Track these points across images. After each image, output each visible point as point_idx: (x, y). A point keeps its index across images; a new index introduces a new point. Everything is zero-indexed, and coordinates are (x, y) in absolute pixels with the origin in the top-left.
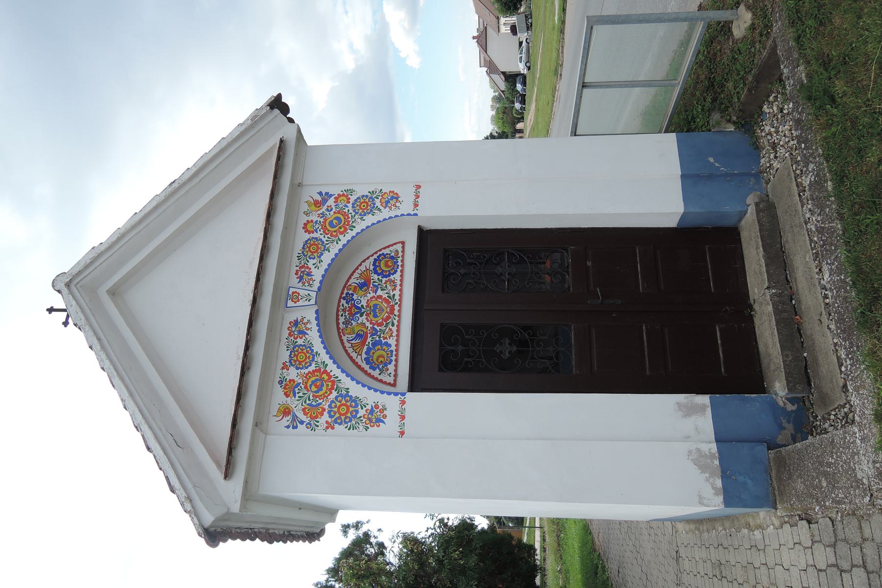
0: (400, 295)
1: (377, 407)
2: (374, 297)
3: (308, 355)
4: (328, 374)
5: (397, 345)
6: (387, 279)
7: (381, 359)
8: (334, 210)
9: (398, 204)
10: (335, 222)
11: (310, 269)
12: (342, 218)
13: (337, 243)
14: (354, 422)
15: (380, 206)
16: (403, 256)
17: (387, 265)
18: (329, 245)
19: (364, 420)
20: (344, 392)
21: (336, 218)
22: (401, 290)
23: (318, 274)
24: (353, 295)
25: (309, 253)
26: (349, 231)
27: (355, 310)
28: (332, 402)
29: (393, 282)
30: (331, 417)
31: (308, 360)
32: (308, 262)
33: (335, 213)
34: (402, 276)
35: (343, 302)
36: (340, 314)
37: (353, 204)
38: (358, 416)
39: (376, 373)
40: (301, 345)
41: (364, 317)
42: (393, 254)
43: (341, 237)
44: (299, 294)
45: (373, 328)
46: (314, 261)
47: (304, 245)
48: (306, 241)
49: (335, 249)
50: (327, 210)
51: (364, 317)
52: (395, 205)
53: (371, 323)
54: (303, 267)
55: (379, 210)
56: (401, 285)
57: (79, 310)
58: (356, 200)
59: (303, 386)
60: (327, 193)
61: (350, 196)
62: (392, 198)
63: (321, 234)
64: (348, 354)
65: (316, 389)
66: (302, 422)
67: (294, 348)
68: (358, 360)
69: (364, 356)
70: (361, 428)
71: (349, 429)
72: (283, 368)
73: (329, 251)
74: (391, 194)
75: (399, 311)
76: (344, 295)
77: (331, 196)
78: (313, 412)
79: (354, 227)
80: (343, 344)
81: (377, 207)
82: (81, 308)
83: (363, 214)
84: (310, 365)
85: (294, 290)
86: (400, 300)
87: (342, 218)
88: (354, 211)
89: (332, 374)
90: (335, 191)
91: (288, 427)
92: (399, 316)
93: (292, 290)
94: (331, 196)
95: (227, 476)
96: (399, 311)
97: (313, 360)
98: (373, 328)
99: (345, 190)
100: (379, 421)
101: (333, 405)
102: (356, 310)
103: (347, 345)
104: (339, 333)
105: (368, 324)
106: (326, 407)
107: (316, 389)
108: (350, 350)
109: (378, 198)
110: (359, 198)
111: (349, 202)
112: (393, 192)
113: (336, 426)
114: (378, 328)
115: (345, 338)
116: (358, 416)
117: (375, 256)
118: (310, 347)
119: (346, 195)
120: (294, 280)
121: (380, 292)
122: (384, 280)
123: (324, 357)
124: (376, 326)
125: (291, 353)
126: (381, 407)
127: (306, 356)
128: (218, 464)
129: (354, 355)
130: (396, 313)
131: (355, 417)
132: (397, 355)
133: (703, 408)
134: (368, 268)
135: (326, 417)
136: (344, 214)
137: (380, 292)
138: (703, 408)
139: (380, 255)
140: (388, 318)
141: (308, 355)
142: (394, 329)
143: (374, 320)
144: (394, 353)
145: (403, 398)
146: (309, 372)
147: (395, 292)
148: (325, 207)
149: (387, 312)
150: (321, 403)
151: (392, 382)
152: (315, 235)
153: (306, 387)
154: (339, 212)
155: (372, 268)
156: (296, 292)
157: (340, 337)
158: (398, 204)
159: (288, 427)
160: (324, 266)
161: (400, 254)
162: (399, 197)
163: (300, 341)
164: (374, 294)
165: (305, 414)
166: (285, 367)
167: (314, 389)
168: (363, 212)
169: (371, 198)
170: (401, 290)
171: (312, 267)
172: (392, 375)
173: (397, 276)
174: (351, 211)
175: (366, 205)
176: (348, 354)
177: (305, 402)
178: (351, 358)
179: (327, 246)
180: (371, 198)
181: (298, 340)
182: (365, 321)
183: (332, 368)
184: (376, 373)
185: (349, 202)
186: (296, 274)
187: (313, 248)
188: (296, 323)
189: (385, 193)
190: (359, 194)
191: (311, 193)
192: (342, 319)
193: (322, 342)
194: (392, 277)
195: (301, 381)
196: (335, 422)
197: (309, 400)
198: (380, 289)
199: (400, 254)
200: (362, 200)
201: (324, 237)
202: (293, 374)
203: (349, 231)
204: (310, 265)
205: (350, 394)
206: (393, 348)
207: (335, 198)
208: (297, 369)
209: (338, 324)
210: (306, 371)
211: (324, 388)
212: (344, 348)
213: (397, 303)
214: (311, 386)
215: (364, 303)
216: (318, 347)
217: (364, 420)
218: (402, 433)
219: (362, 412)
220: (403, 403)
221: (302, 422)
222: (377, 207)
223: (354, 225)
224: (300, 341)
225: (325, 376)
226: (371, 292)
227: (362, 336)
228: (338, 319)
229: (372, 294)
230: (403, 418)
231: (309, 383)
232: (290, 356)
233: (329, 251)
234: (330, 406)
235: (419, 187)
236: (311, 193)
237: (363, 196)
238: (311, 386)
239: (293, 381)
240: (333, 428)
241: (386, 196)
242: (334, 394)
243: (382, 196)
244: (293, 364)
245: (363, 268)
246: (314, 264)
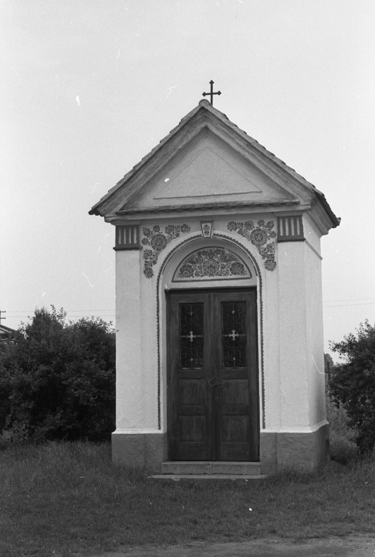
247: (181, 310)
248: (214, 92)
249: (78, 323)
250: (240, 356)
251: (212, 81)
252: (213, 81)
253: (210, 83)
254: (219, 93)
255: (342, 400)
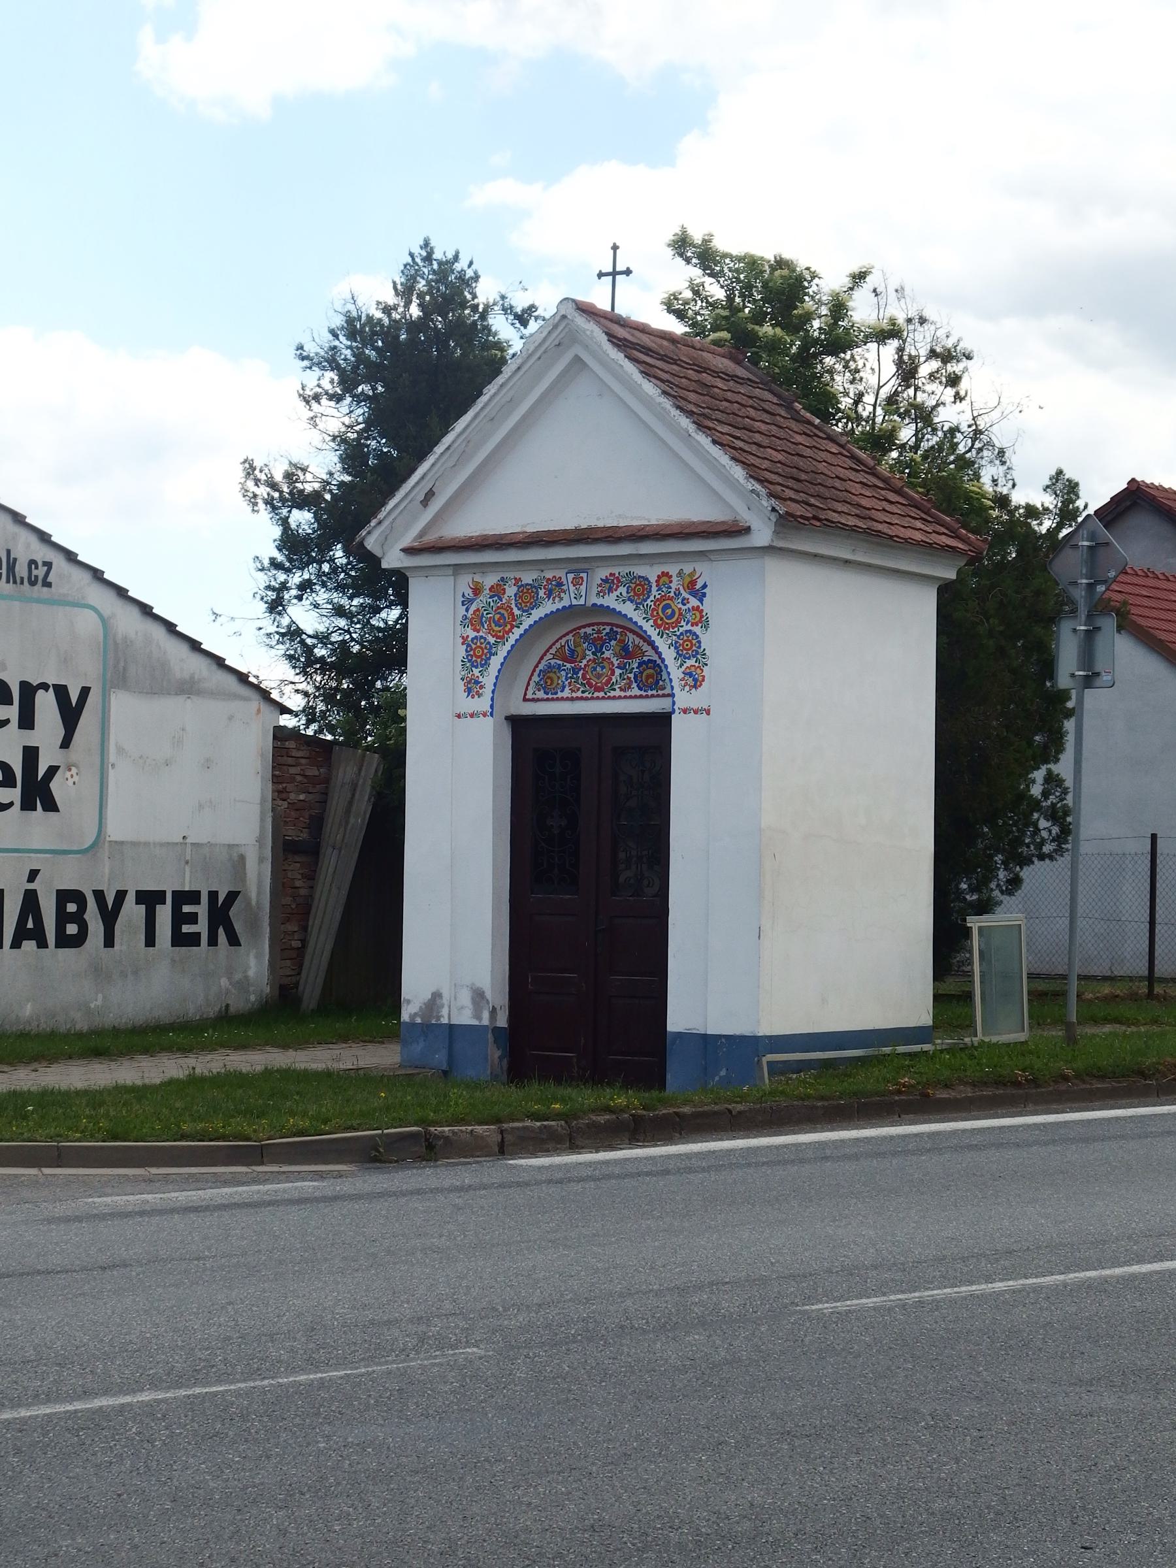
0: (614, 698)
1: (482, 687)
2: (613, 665)
3: (528, 604)
4: (511, 630)
5: (562, 699)
6: (632, 679)
7: (549, 682)
8: (684, 608)
9: (687, 688)
10: (669, 611)
11: (616, 590)
12: (674, 620)
13: (644, 618)
14: (468, 665)
15: (685, 665)
16: (658, 696)
17: (648, 676)
18: (642, 608)
19: (469, 675)
20: (494, 650)
21: (673, 612)
22: (620, 697)
23: (610, 601)
24: (615, 640)
25: (633, 586)
26: (658, 630)
27: (599, 645)
28: (485, 639)
29: (629, 687)
30: (473, 639)
31: (523, 605)
32: (624, 586)
33: (680, 609)
34: (636, 697)
35: (608, 629)
36: (595, 628)
37: (690, 631)
38: (473, 669)
39: (536, 678)
40: (538, 595)
41: (592, 657)
42: (661, 683)
43: (651, 622)
44: (581, 584)
45: (580, 669)
46: (625, 594)
47: (643, 577)
48: (647, 579)
49: (637, 617)
50: (684, 599)
51: (592, 657)
52: (686, 684)
53: (585, 665)
54: (619, 581)
55: (681, 666)
56: (625, 697)
57: (536, 344)
58: (695, 634)
59: (499, 605)
60: (704, 595)
61: (700, 625)
62: (695, 680)
63: (655, 596)
64: (554, 644)
65: (496, 619)
66: (467, 610)
67: (535, 587)
68: (549, 656)
69: (553, 662)
70: (463, 673)
71: (462, 661)
72: (515, 579)
73: (635, 610)
74: (700, 678)
75: (598, 698)
76: (615, 629)
77: (701, 601)
78: (475, 621)
79: (661, 637)
80: (564, 636)
81: (685, 662)
82: (540, 345)
83: (678, 645)
84: (519, 609)
85: (585, 579)
86: (609, 698)
87: (674, 620)
88: (682, 634)
89: (511, 634)
90: (706, 607)
91: (463, 596)
92: (592, 698)
93: (584, 575)
94: (701, 601)
95: (403, 550)
96: (598, 698)
97: (524, 611)
98: (580, 669)
99: (707, 618)
100: (469, 691)
101: (482, 640)
102: (599, 646)
103: (563, 641)
104: (574, 630)
105: (585, 662)
106: (481, 634)
107: (496, 619)
108: (558, 645)
109: (696, 662)
110: (697, 637)
111: (692, 625)
112: (703, 680)
113: (465, 646)
114: (580, 675)
115: (570, 637)
116: (473, 669)
117: (659, 661)
118: (536, 605)
119: (704, 622)
120: (603, 573)
121: (618, 672)
122: (632, 676)
123: (527, 623)
124: (582, 672)
125: (531, 584)
126: (481, 691)
127: (527, 602)
128: (422, 534)
129: (553, 651)
130: (596, 694)
131: (473, 666)
132: (553, 699)
133: (479, 1018)
134: (646, 654)
135: (472, 634)
136: (678, 622)
137: (618, 672)
138: (478, 1016)
139: (660, 667)
140: (590, 685)
141: (528, 604)
142: (579, 694)
143: (589, 669)
144: (555, 696)
145: (489, 714)
146: (512, 609)
147: (618, 690)
148: (687, 596)
149: (597, 683)
150: (484, 627)
151: (527, 697)
152: (654, 588)
153: (498, 608)
154: (680, 614)
155: (645, 659)
156: (583, 581)
157: (571, 632)
158: (687, 688)
159: (463, 596)
160: (619, 607)
161: (660, 692)
162: (696, 688)
163: (541, 593)
164: (616, 665)
165: (475, 612)
166: (518, 580)
167: (497, 617)
168: (680, 645)
169: (697, 653)
170: (620, 697)
171: (618, 593)
172: (534, 696)
173: (636, 691)
174: (681, 630)
175: (689, 648)
176: (554, 644)
177: (485, 610)
178: (550, 647)
179: (641, 606)
180: (697, 653)
181: (543, 590)
182: (588, 658)
183: (517, 632)
184: (536, 678)
185: (692, 625)
186: (611, 575)
187: (638, 589)
188: (560, 584)
189: (702, 670)
190: (702, 638)
191: (705, 572)
192: (589, 630)
193: (541, 618)
194: (634, 685)
195: (504, 601)
196: (468, 645)
197: (487, 614)
198: (621, 671)
199: (660, 692)
200: (694, 642)
201: (652, 601)
202: (511, 591)
203: (658, 630)
204: (623, 590)
205: (492, 657)
206: (560, 695)
207: (698, 607)
208: (515, 595)
209: (584, 627)
210: (513, 606)
211: (497, 628)
212: (560, 638)
213: (606, 694)
214: (499, 613)
215: (607, 654)
216: (537, 614)
217: (469, 675)
218: (459, 716)
219: (476, 672)
220: (485, 715)
221: (467, 610)
222: (685, 662)
223: (665, 636)
224: (541, 593)
225: (509, 626)
226: (618, 662)
227: (572, 657)
228: (589, 625)
229: (616, 663)
230: (472, 716)
231: (502, 611)
232: (527, 584)
233: (635, 610)
234: (481, 637)
235: (708, 712)
236: (705, 572)
237: (699, 642)
238: (499, 613)
239: (504, 593)
240: (463, 644)
241: (699, 671)
242: (492, 640)
243: (699, 667)
244: (520, 590)
245: (645, 647)
246: (621, 594)
247: (269, 820)
248: (618, 269)
249: (241, 980)
250: (546, 777)
251: (614, 244)
252: (617, 244)
253: (612, 248)
254: (628, 272)
255: (559, 1129)
